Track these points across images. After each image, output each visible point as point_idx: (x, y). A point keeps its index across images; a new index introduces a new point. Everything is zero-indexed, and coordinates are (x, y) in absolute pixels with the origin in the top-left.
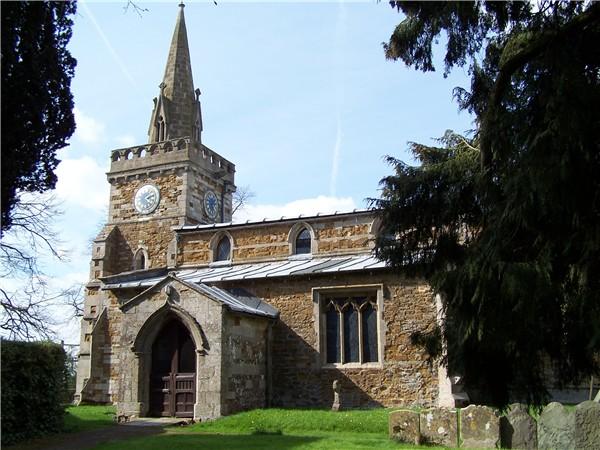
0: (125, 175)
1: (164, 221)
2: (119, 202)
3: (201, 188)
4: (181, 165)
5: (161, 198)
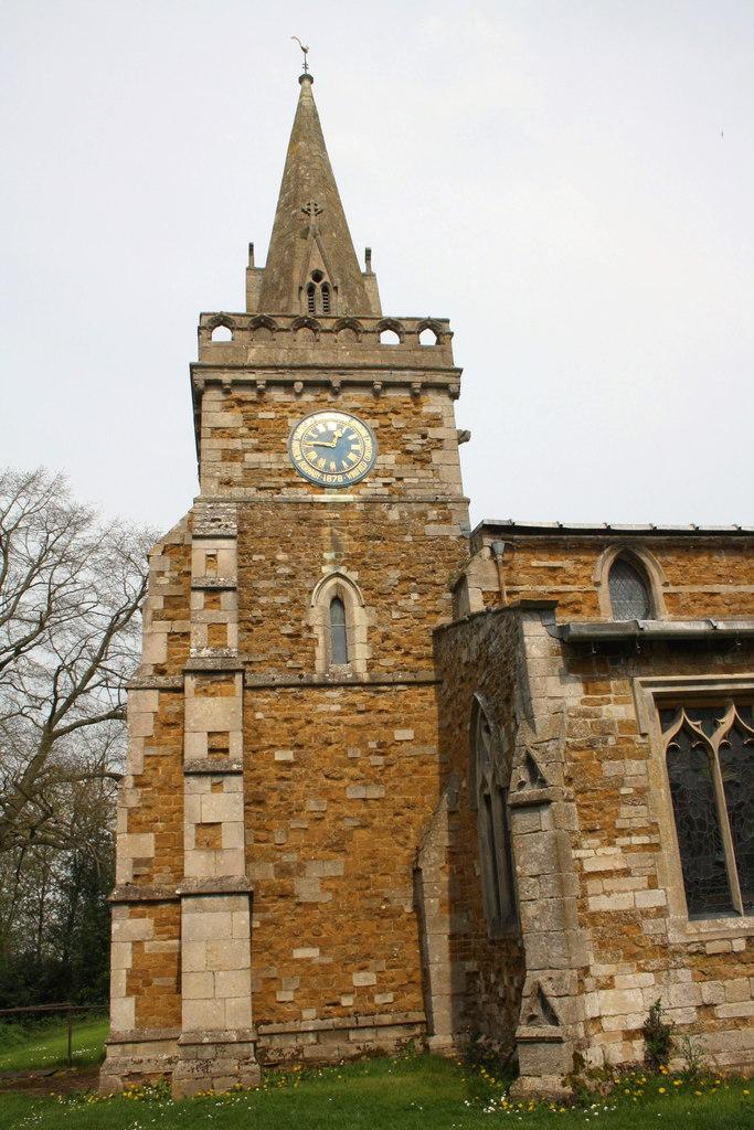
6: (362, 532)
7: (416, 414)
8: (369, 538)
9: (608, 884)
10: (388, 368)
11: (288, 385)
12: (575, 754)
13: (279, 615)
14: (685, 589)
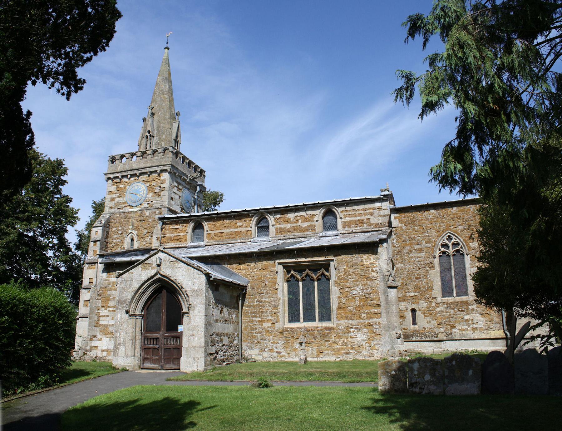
0: (119, 175)
1: (150, 211)
2: (114, 196)
4: (165, 168)
6: (139, 219)
7: (159, 180)
8: (141, 221)
9: (104, 318)
10: (151, 167)
11: (126, 176)
12: (103, 289)
13: (118, 245)
14: (213, 232)
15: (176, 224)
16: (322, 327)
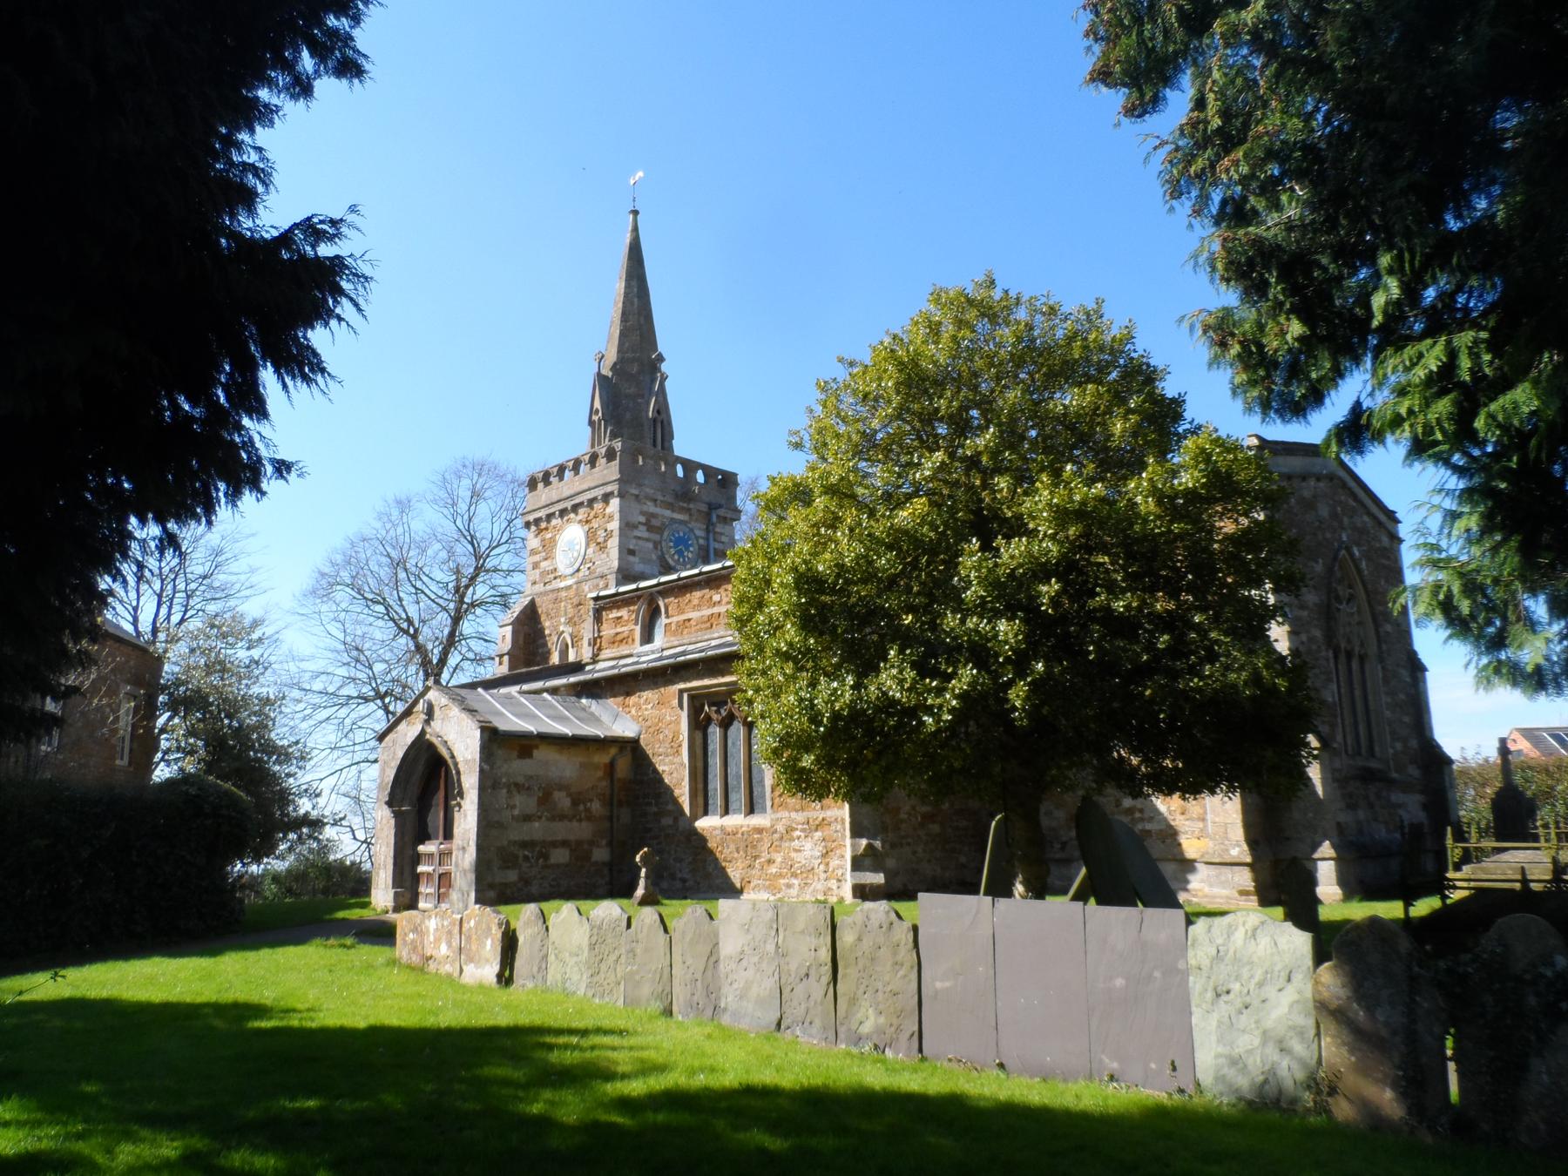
1: (589, 583)
2: (537, 558)
3: (655, 522)
5: (587, 545)
15: (618, 608)
16: (748, 826)
